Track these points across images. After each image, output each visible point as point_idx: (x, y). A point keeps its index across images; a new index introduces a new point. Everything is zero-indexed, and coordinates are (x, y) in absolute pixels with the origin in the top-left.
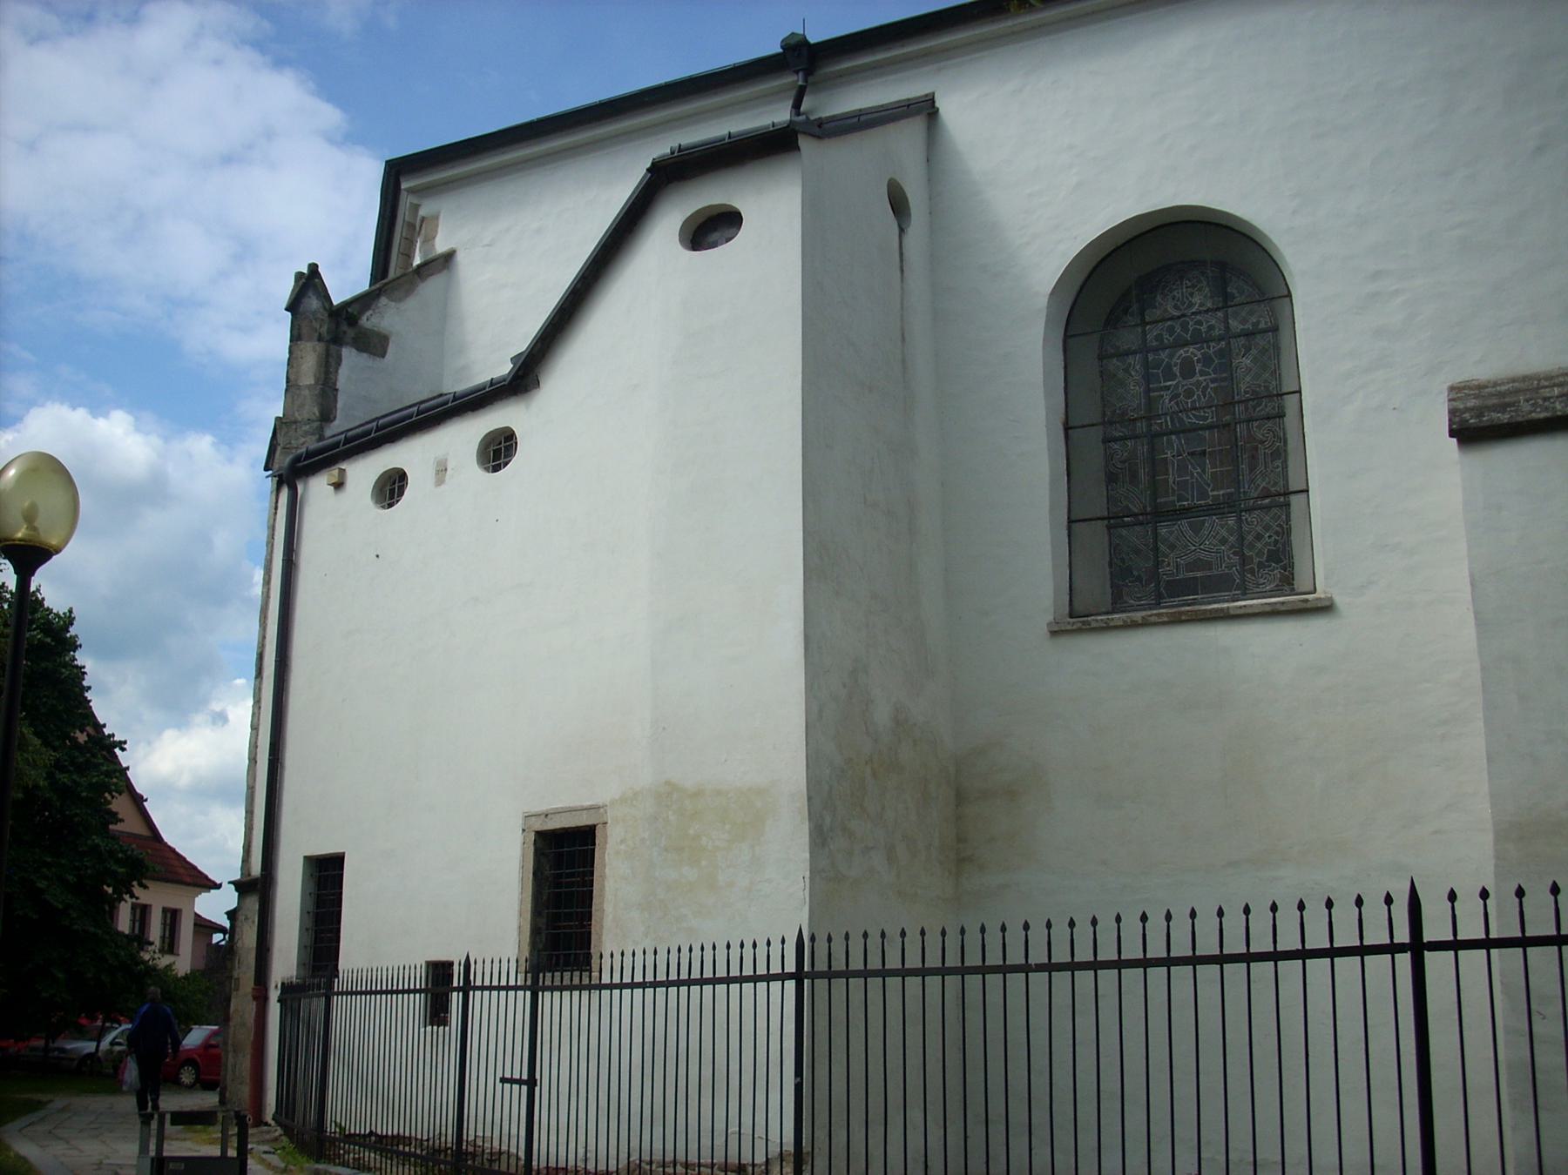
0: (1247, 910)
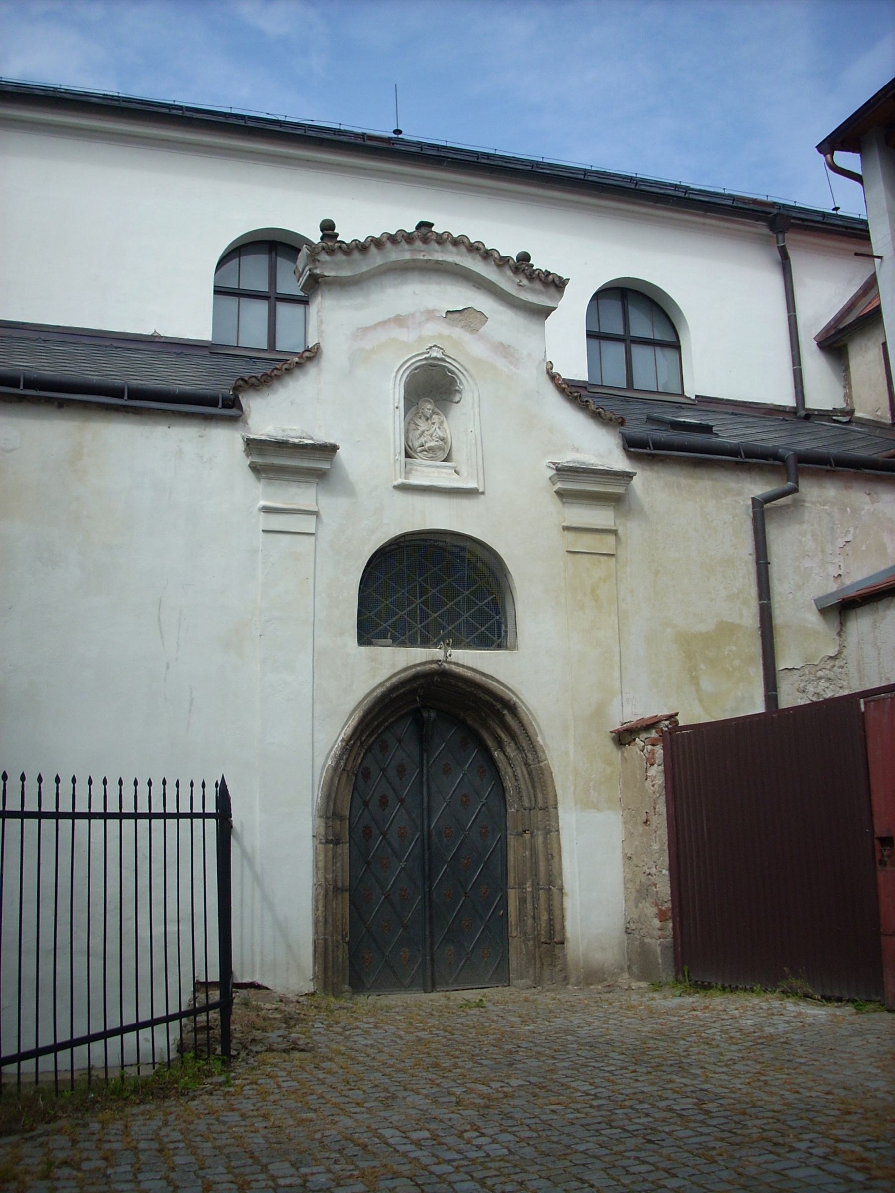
0: (121, 783)
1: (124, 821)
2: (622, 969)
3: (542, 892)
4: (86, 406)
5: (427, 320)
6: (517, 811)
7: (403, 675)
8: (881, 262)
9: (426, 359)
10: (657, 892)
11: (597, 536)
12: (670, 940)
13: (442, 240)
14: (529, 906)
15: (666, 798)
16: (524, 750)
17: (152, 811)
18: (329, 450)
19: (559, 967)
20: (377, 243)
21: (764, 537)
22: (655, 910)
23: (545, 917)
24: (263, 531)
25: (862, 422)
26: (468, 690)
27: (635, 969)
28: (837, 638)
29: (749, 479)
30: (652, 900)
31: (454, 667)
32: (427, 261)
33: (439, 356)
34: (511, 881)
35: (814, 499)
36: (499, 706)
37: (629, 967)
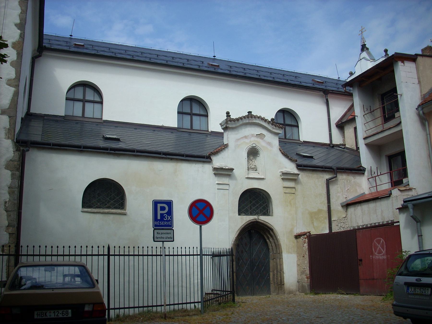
1: (58, 257)
2: (297, 291)
3: (279, 273)
4: (177, 160)
5: (252, 137)
6: (272, 254)
7: (248, 222)
8: (357, 117)
9: (252, 146)
10: (306, 273)
11: (291, 189)
12: (309, 283)
13: (255, 117)
14: (275, 276)
15: (308, 251)
16: (274, 240)
17: (170, 254)
18: (232, 170)
19: (282, 290)
20: (241, 118)
21: (329, 189)
22: (306, 277)
23: (279, 279)
24: (217, 189)
25: (348, 149)
26: (262, 225)
27: (300, 291)
28: (345, 213)
29: (325, 174)
30: (305, 274)
31: (259, 220)
32: (252, 122)
33: (255, 146)
34: (271, 270)
35: (340, 179)
36: (269, 229)
37: (299, 290)
